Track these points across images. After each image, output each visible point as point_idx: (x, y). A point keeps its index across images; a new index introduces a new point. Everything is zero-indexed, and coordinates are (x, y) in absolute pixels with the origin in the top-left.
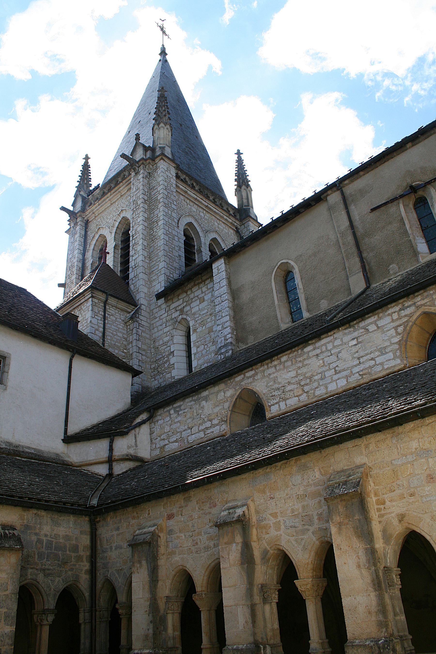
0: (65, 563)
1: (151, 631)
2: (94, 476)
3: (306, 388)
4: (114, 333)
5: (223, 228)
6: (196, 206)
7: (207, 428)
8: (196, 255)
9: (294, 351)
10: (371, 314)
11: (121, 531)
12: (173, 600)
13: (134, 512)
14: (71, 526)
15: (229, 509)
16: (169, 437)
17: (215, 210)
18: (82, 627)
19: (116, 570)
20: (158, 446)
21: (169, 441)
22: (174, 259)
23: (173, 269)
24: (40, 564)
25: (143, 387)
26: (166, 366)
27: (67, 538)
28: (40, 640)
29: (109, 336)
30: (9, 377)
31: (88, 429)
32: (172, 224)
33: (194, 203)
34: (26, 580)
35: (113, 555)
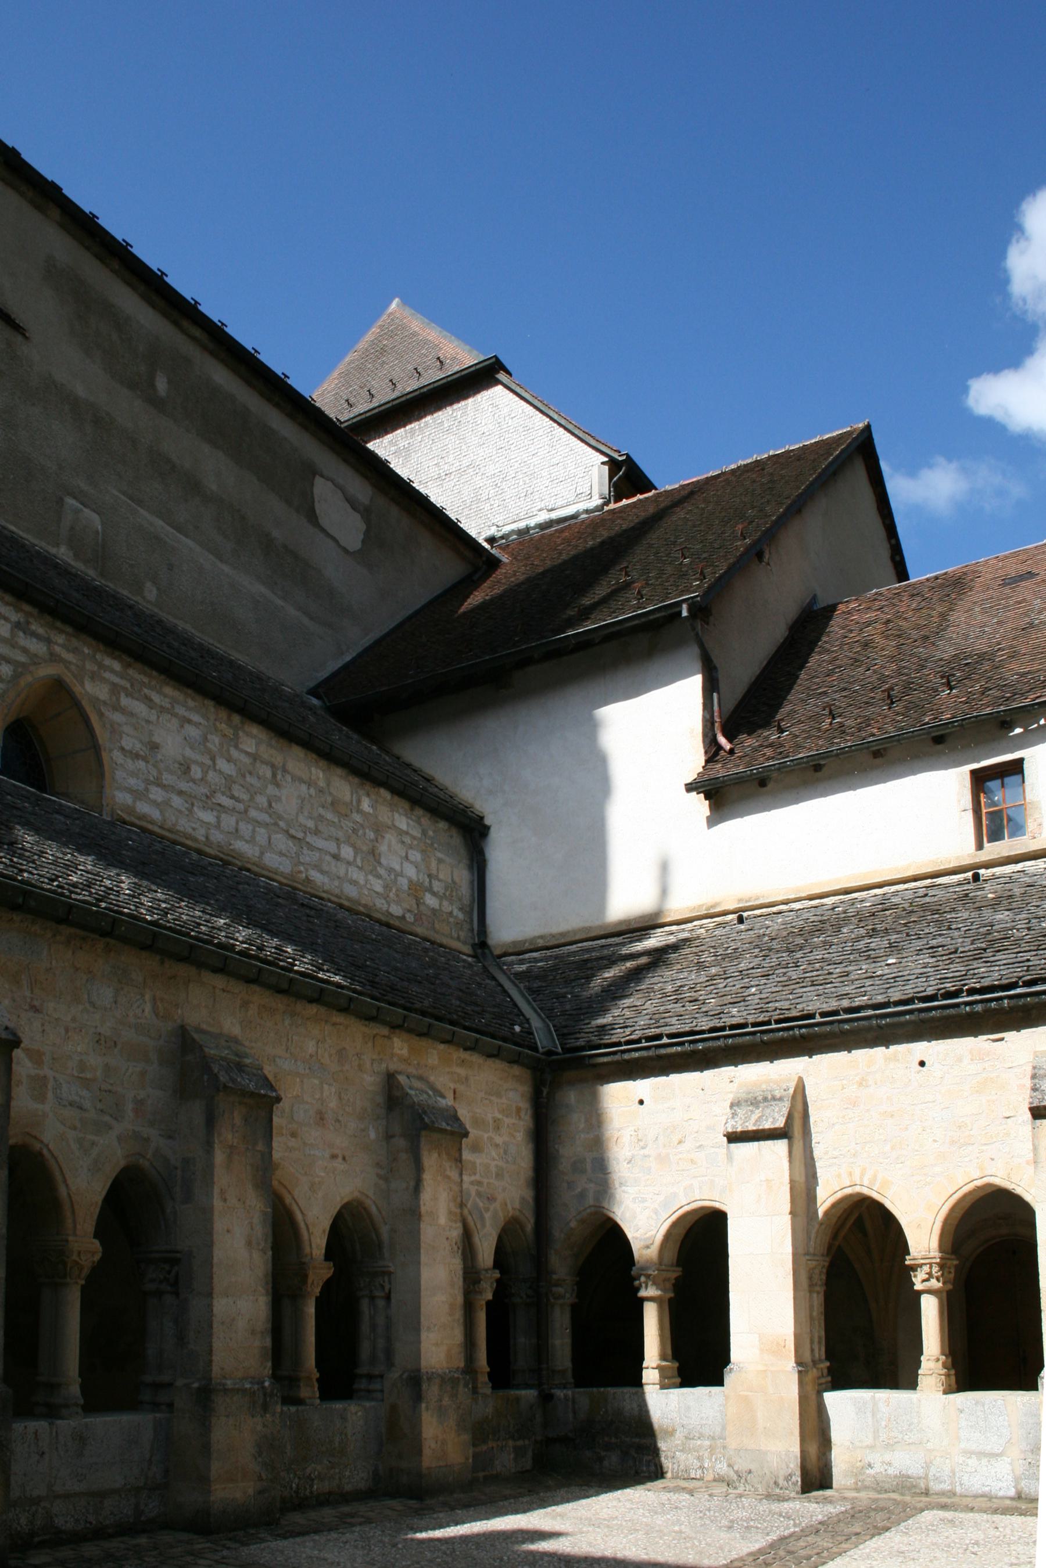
10: (69, 630)
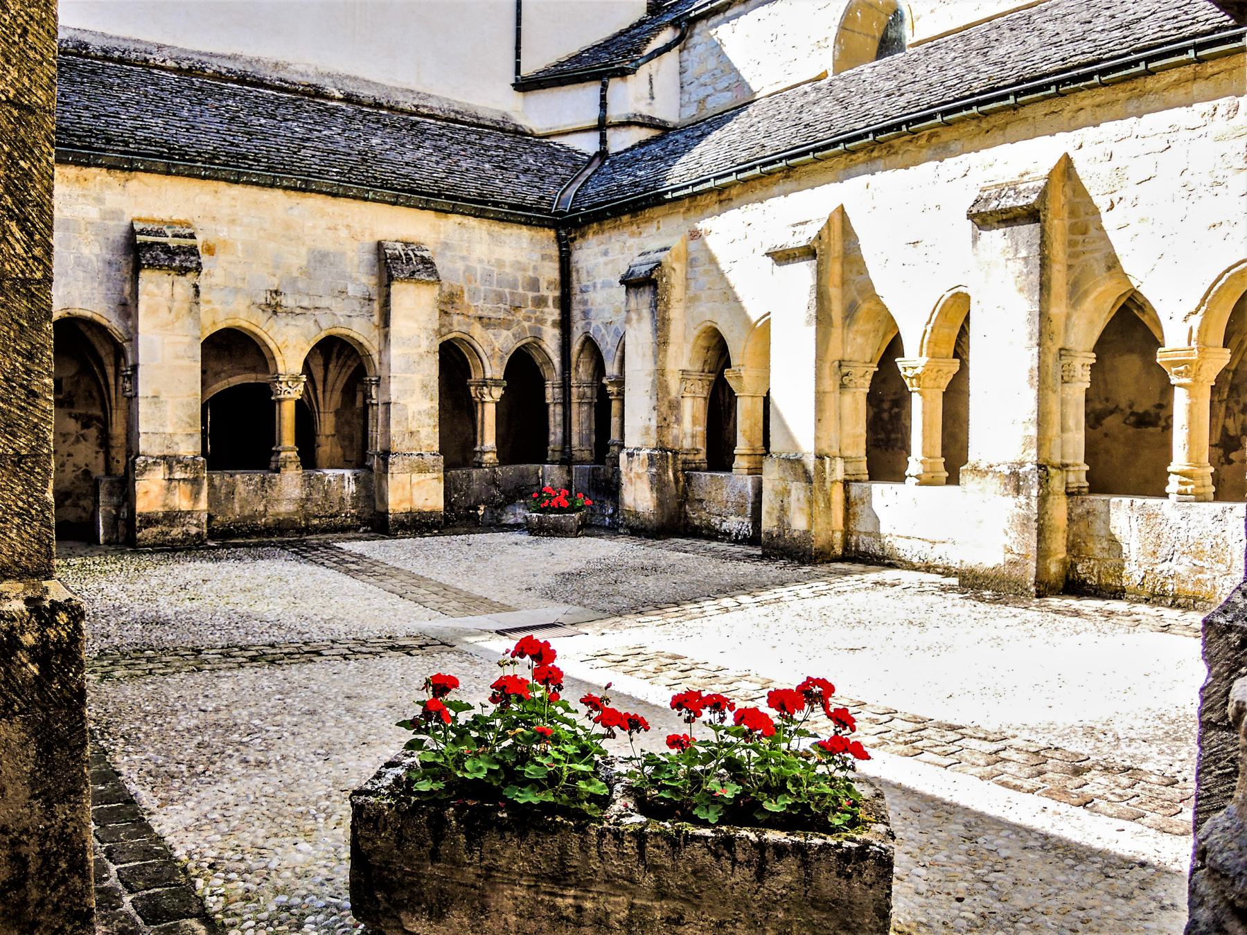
1: (654, 423)
2: (571, 154)
11: (610, 258)
14: (525, 245)
18: (551, 408)
20: (694, 97)
28: (483, 423)
31: (561, 64)
34: (450, 332)
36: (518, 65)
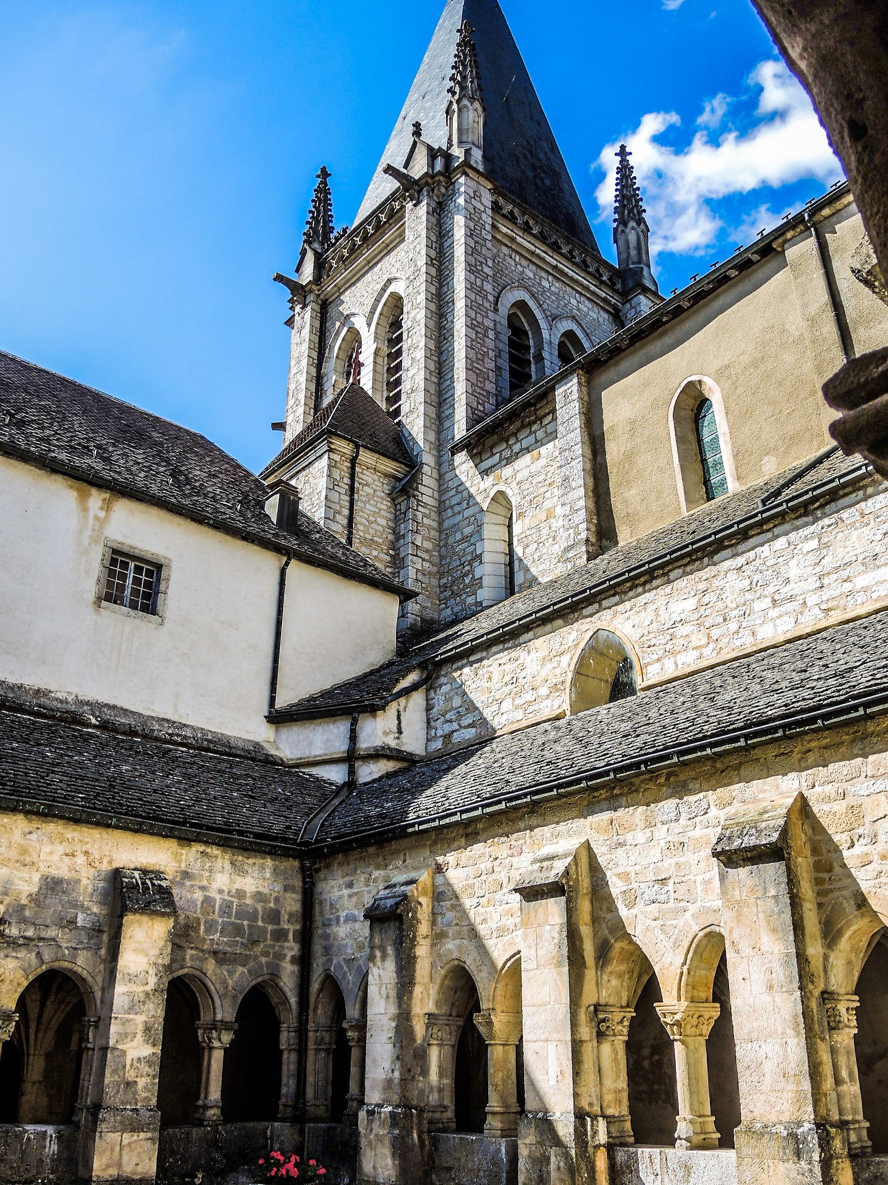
0: (255, 943)
1: (397, 1074)
3: (715, 633)
4: (371, 518)
5: (589, 309)
6: (534, 268)
7: (529, 703)
8: (533, 366)
9: (696, 560)
11: (355, 890)
12: (441, 1022)
13: (378, 856)
14: (268, 875)
15: (541, 861)
16: (460, 716)
17: (571, 273)
18: (285, 1055)
19: (344, 959)
20: (440, 732)
21: (459, 725)
22: (486, 376)
23: (483, 396)
24: (208, 942)
25: (423, 620)
26: (467, 581)
27: (259, 896)
29: (362, 524)
30: (168, 601)
32: (482, 305)
33: (530, 261)
34: (182, 967)
35: (342, 931)
36: (272, 700)
